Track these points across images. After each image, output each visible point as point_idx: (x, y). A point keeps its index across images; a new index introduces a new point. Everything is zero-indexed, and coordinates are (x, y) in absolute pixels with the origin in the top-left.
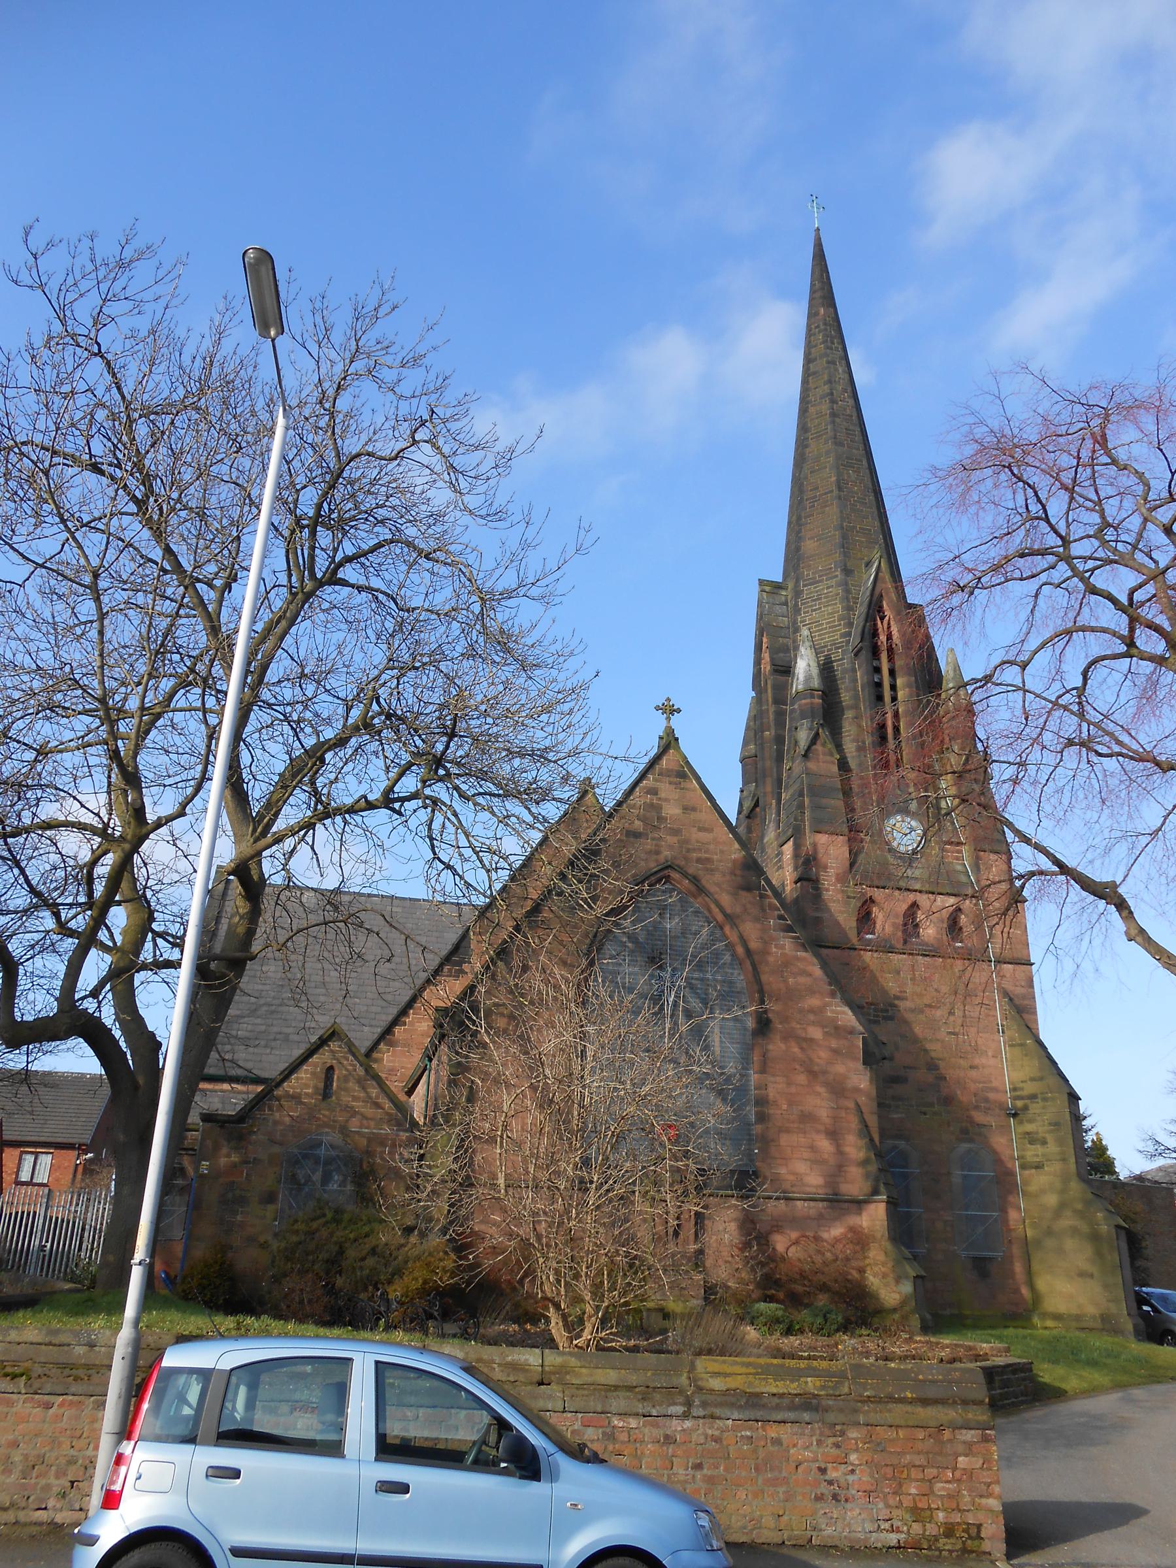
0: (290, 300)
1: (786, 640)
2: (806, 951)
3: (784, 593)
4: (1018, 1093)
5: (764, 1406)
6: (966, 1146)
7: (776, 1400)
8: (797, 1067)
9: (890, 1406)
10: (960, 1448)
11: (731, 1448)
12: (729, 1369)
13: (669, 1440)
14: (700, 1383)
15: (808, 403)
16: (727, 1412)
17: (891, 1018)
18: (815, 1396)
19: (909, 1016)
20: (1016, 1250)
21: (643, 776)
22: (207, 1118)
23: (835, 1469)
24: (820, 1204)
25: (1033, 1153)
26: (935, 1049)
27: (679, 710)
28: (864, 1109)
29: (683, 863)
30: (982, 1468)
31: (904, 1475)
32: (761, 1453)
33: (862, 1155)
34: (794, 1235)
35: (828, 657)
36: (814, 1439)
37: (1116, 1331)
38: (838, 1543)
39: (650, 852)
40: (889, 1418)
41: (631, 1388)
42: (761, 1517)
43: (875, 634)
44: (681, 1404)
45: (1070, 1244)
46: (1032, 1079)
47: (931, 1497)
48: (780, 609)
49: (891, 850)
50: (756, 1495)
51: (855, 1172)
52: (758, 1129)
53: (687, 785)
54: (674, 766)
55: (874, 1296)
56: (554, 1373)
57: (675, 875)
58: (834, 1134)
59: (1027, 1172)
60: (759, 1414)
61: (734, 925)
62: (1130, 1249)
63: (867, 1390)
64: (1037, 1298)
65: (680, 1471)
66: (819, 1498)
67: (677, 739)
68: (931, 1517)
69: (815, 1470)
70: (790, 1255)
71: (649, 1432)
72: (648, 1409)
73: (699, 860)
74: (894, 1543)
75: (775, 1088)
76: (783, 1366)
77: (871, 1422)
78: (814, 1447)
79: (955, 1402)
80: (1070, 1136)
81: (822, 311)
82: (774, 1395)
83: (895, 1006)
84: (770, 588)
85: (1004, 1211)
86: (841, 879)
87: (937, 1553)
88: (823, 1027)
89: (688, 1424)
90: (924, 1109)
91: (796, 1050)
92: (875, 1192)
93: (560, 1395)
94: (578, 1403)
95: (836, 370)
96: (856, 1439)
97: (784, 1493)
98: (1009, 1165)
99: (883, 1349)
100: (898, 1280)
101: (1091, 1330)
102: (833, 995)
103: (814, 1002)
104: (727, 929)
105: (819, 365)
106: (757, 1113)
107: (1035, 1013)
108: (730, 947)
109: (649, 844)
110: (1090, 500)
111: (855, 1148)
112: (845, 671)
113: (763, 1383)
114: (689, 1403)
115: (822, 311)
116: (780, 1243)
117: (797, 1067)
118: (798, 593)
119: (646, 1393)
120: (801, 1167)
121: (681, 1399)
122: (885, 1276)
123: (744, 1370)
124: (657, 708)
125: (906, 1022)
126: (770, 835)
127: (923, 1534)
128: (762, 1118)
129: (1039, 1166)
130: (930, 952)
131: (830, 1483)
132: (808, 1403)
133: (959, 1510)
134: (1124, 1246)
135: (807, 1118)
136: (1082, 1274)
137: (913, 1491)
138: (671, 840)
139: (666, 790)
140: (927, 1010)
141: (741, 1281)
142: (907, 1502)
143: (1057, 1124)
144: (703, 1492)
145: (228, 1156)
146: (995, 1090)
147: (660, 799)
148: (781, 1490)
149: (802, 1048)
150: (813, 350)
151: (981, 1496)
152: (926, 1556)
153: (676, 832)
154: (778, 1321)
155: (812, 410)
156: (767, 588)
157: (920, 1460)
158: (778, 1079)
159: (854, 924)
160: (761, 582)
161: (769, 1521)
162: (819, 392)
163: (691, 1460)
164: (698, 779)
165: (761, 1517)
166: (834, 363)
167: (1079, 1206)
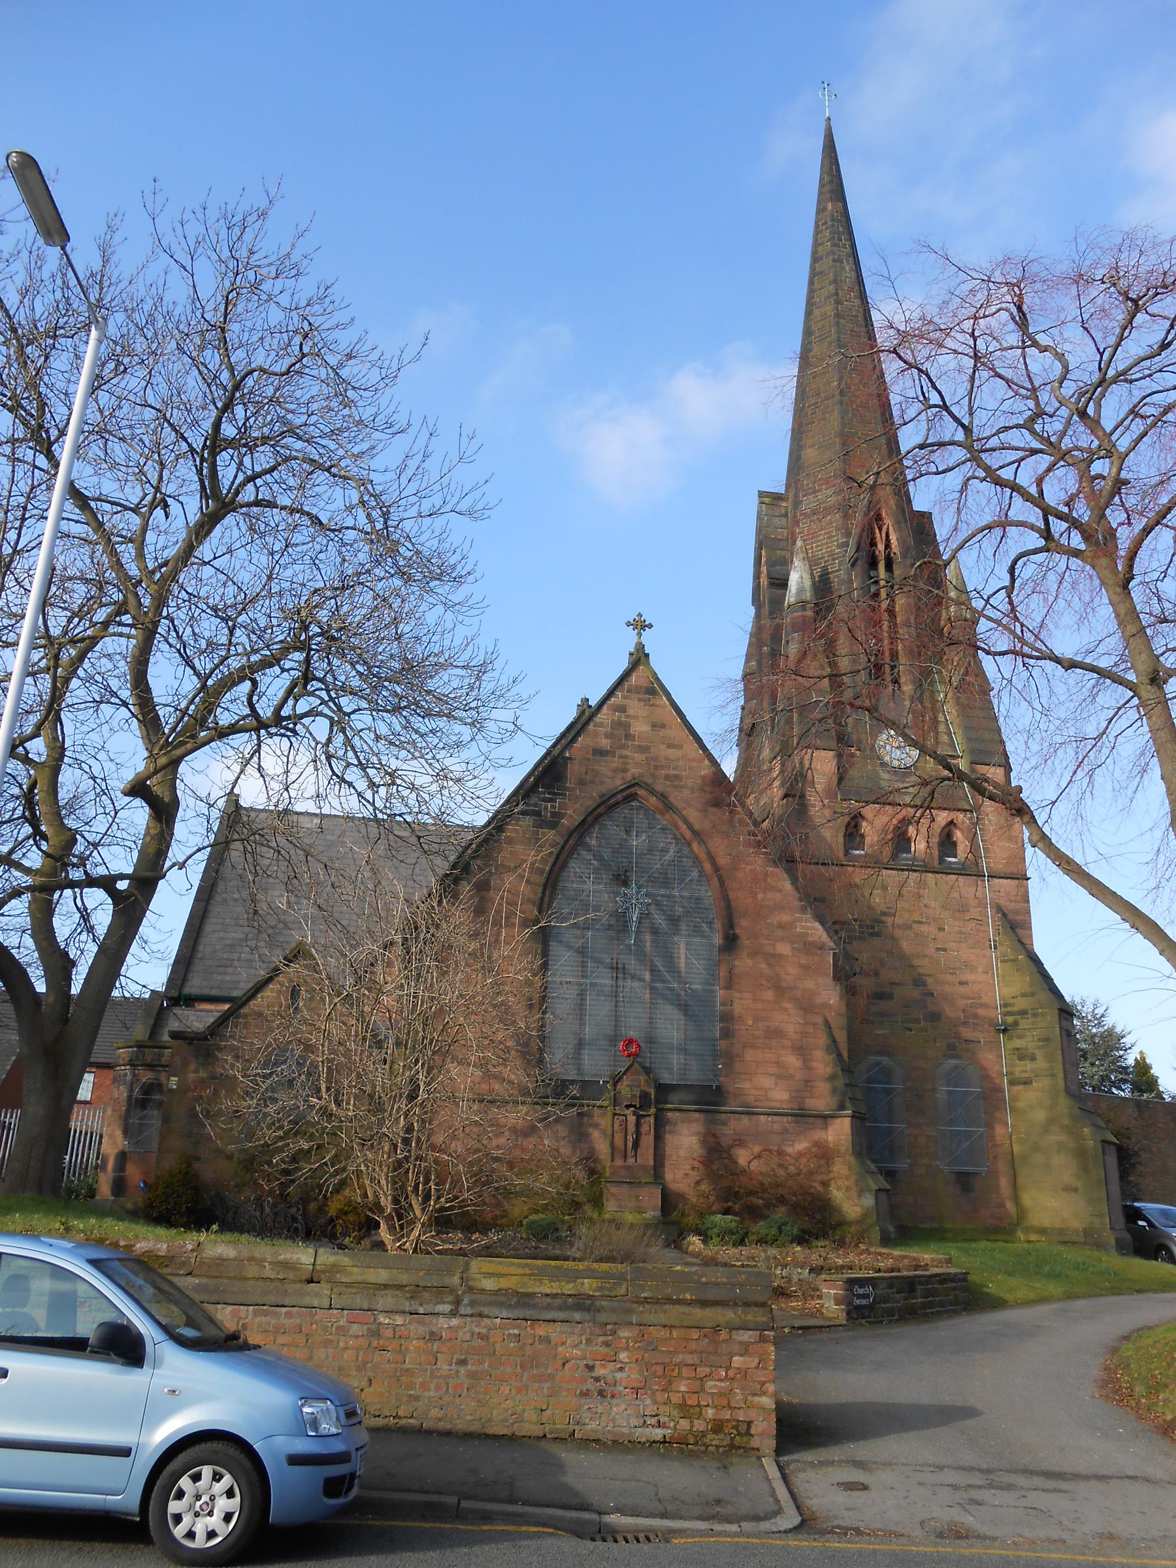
0: (157, 212)
1: (783, 553)
2: (777, 866)
3: (784, 504)
4: (1009, 1009)
5: (535, 1306)
6: (954, 1062)
7: (549, 1300)
8: (764, 982)
9: (667, 1307)
10: (736, 1348)
11: (498, 1346)
12: (502, 1269)
13: (434, 1337)
14: (471, 1283)
15: (813, 304)
16: (495, 1311)
17: (878, 935)
18: (590, 1297)
19: (898, 933)
20: (1002, 1166)
21: (611, 693)
22: (175, 1035)
23: (603, 1366)
24: (785, 1119)
25: (1023, 1068)
26: (924, 966)
27: (650, 626)
28: (833, 1025)
29: (649, 780)
30: (757, 1367)
31: (675, 1374)
32: (529, 1351)
33: (829, 1070)
34: (757, 1149)
35: (825, 568)
36: (584, 1338)
37: (1099, 1245)
38: (601, 1437)
39: (616, 771)
40: (662, 1318)
41: (400, 1287)
42: (524, 1411)
43: (873, 544)
44: (449, 1303)
45: (1058, 1160)
46: (1023, 995)
47: (701, 1395)
48: (778, 522)
49: (884, 765)
50: (519, 1391)
51: (823, 1088)
52: (723, 1044)
53: (658, 702)
54: (643, 683)
55: (837, 1210)
56: (324, 1272)
57: (641, 792)
58: (801, 1050)
59: (1016, 1088)
60: (528, 1313)
61: (702, 842)
62: (1120, 1164)
63: (644, 1291)
64: (1022, 1213)
65: (444, 1367)
66: (585, 1394)
67: (647, 655)
68: (701, 1413)
69: (582, 1367)
70: (752, 1168)
71: (415, 1329)
72: (415, 1306)
73: (667, 777)
74: (659, 1437)
75: (742, 1004)
76: (560, 1268)
77: (644, 1322)
78: (583, 1346)
79: (736, 1304)
80: (1059, 1052)
81: (830, 206)
82: (547, 1295)
83: (882, 922)
84: (769, 500)
85: (990, 1126)
86: (830, 794)
87: (703, 1448)
88: (792, 942)
89: (454, 1322)
90: (909, 1025)
91: (763, 965)
92: (842, 1107)
93: (328, 1293)
94: (345, 1301)
95: (843, 268)
96: (627, 1339)
97: (549, 1388)
98: (998, 1081)
99: (825, 1259)
100: (861, 1193)
101: (1073, 1243)
102: (803, 910)
103: (785, 918)
104: (695, 845)
105: (826, 264)
106: (721, 1029)
107: (1030, 928)
108: (697, 861)
109: (616, 763)
110: (1024, 388)
111: (823, 1064)
112: (842, 582)
113: (538, 1283)
114: (457, 1302)
115: (830, 206)
116: (742, 1157)
117: (764, 982)
118: (797, 503)
119: (416, 1291)
120: (766, 1082)
121: (450, 1298)
122: (848, 1189)
123: (520, 1271)
124: (629, 624)
125: (893, 938)
126: (766, 753)
127: (691, 1430)
128: (727, 1034)
129: (1027, 1082)
130: (926, 868)
131: (597, 1379)
132: (582, 1303)
133: (730, 1408)
134: (1112, 1160)
135: (775, 1033)
136: (1067, 1189)
137: (683, 1388)
138: (640, 757)
139: (635, 707)
140: (915, 926)
141: (702, 1195)
142: (676, 1399)
143: (1046, 1040)
144: (465, 1386)
145: (196, 1071)
146: (985, 1006)
147: (628, 716)
148: (546, 1385)
149: (769, 965)
150: (820, 249)
151: (755, 1395)
152: (692, 1450)
153: (643, 749)
154: (731, 1233)
155: (816, 312)
156: (767, 500)
157: (689, 1359)
158: (746, 995)
159: (841, 840)
160: (761, 494)
161: (531, 1415)
162: (824, 292)
163: (455, 1357)
164: (668, 695)
165: (524, 1411)
166: (839, 261)
167: (1066, 1122)
